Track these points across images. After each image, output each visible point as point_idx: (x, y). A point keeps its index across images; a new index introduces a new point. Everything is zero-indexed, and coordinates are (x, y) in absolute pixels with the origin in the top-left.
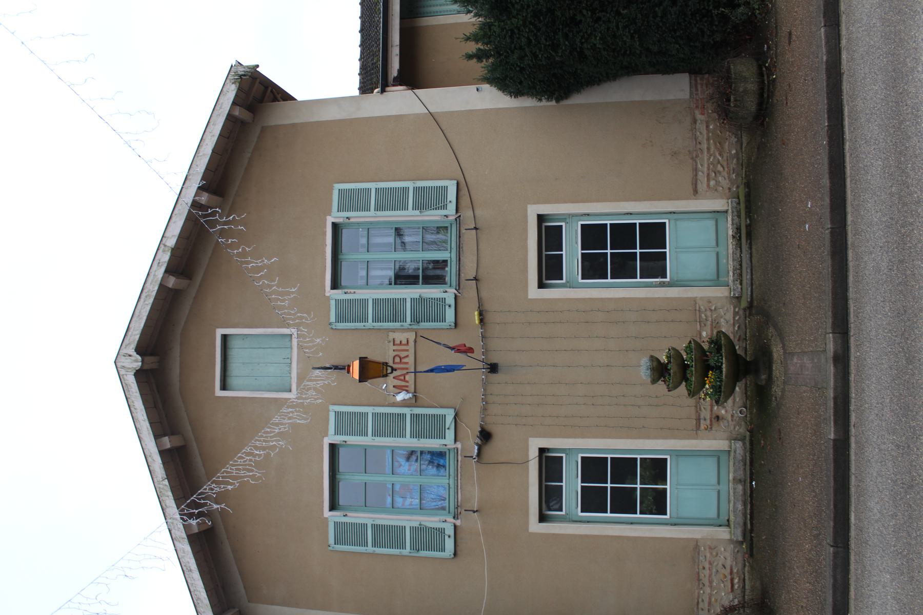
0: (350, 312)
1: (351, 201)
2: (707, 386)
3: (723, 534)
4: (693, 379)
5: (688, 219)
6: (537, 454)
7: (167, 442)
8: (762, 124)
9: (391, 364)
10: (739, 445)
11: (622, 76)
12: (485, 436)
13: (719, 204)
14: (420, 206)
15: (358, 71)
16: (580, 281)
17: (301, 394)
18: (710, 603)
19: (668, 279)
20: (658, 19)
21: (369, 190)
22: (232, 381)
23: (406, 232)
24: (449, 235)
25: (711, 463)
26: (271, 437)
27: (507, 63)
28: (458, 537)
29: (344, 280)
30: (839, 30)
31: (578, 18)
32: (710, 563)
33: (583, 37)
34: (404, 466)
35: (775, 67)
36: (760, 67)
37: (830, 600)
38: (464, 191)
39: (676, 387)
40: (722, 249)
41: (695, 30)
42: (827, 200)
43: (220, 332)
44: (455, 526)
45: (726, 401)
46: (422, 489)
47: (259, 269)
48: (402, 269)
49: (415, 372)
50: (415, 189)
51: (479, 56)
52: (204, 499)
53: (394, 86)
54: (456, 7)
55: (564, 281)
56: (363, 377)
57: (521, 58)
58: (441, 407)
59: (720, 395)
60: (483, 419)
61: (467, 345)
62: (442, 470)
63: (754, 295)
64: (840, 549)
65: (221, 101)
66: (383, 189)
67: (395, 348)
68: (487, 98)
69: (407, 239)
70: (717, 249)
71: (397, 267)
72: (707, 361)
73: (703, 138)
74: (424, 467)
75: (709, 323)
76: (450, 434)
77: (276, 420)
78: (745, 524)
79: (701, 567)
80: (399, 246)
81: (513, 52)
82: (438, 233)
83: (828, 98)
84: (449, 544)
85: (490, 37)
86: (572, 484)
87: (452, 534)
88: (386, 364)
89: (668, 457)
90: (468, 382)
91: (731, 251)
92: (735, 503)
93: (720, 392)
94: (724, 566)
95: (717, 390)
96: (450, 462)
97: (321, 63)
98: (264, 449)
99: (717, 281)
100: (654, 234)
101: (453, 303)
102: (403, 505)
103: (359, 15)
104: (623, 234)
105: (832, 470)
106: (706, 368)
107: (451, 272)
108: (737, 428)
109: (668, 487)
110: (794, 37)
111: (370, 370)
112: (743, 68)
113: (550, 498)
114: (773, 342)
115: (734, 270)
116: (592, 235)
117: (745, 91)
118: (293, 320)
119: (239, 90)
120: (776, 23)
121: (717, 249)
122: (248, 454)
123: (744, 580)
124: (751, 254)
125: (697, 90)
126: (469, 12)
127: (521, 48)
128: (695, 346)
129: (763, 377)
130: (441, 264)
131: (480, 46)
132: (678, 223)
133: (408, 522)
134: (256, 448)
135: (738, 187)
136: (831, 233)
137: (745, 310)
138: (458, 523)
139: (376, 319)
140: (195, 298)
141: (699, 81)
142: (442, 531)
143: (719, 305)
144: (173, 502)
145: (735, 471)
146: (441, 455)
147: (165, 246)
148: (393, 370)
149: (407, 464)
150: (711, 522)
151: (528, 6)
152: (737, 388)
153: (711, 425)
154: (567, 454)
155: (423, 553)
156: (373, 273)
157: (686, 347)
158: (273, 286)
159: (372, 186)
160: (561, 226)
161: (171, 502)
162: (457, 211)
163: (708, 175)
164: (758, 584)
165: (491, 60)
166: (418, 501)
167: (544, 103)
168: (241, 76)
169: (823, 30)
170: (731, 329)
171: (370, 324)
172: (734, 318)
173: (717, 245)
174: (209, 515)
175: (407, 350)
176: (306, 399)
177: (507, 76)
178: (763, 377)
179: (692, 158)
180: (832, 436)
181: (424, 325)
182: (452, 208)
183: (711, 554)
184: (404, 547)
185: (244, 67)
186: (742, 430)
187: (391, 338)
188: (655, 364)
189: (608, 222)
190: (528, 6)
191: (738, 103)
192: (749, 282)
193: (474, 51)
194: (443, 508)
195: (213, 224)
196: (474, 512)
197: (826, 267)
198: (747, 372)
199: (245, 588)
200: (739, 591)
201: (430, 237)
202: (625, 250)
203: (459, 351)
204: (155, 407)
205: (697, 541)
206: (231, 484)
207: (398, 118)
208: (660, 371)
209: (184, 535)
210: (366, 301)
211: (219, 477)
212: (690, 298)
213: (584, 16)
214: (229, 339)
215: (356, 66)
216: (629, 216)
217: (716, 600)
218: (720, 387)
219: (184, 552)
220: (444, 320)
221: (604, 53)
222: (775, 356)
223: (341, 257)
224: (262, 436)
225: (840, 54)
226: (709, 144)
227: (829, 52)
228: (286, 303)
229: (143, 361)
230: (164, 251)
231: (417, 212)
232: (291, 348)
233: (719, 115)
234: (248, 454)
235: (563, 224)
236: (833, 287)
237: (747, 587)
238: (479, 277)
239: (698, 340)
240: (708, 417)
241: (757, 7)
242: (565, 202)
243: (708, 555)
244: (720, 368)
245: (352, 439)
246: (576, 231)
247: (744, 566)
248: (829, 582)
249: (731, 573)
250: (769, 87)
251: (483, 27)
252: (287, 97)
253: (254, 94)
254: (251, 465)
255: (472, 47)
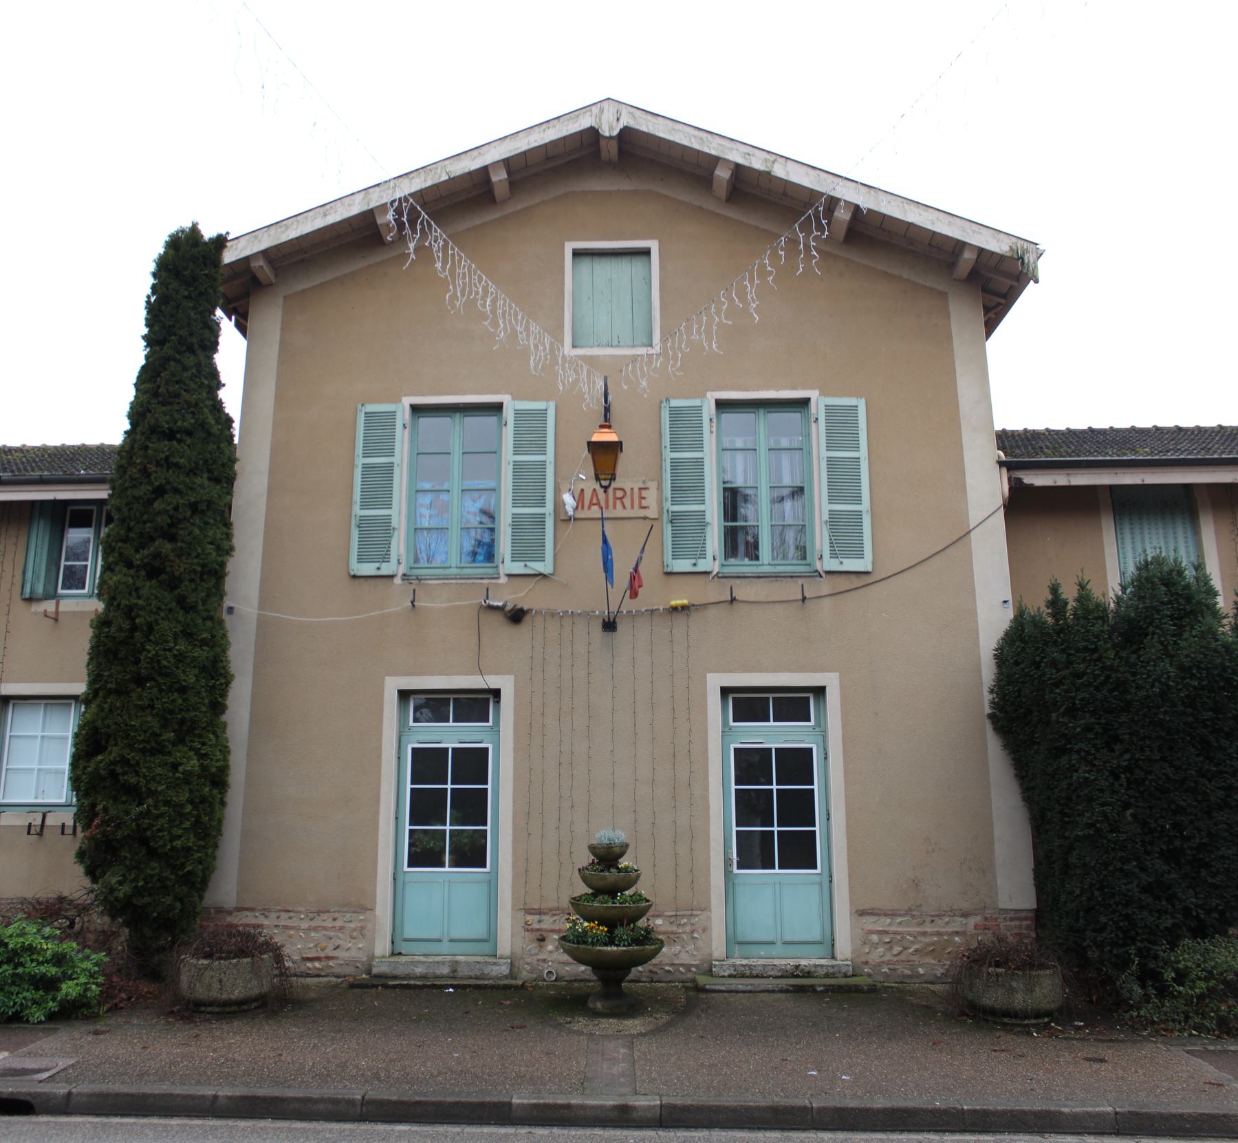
0: (685, 426)
1: (841, 423)
2: (586, 924)
3: (382, 947)
4: (596, 904)
5: (822, 902)
6: (492, 687)
7: (499, 177)
8: (963, 1014)
9: (614, 485)
10: (505, 970)
11: (1030, 809)
12: (517, 616)
13: (845, 949)
14: (834, 520)
15: (1030, 427)
16: (732, 747)
17: (570, 362)
18: (286, 927)
19: (736, 871)
20: (1119, 865)
21: (857, 449)
22: (586, 265)
23: (798, 503)
24: (795, 562)
25: (479, 931)
26: (510, 321)
27: (1046, 644)
28: (378, 580)
29: (729, 417)
30: (1110, 1134)
31: (1118, 747)
32: (341, 928)
33: (1088, 753)
34: (473, 506)
35: (1050, 1037)
36: (1048, 1014)
37: (290, 1093)
38: (857, 582)
39: (584, 879)
40: (779, 949)
41: (1103, 919)
42: (853, 1104)
43: (654, 245)
44: (392, 577)
45: (566, 951)
46: (442, 530)
47: (742, 295)
48: (746, 499)
49: (602, 519)
50: (859, 514)
51: (1056, 603)
52: (422, 229)
53: (1009, 479)
54: (1131, 569)
55: (732, 723)
56: (594, 447)
57: (1054, 664)
58: (555, 556)
59: (574, 943)
60: (539, 612)
61: (640, 591)
62: (469, 559)
63: (714, 995)
64: (359, 1109)
65: (984, 230)
66: (858, 469)
67: (636, 491)
68: (993, 618)
69: (788, 505)
70: (779, 943)
71: (748, 492)
72: (622, 925)
73: (940, 926)
74: (473, 533)
75: (675, 929)
76: (518, 568)
77: (534, 328)
78: (395, 977)
79: (336, 915)
80: (777, 493)
81: (1063, 651)
82: (797, 548)
83: (1004, 1112)
84: (368, 569)
85: (1084, 618)
86: (451, 735)
87: (382, 572)
88: (613, 478)
89: (488, 869)
90: (588, 590)
91: (776, 962)
92: (424, 963)
93: (578, 943)
94: (337, 947)
95: (581, 938)
96: (481, 569)
97: (1045, 372)
98: (494, 312)
99: (733, 941)
100: (800, 852)
101: (699, 569)
102: (421, 505)
103: (1116, 426)
104: (800, 808)
105: (469, 1099)
106: (611, 923)
107: (742, 565)
108: (528, 968)
109: (447, 869)
110: (1096, 1066)
111: (605, 457)
112: (1046, 988)
113: (434, 705)
114: (648, 1019)
115: (750, 967)
116: (797, 764)
117: (1012, 990)
118: (672, 348)
119: (1001, 257)
120: (1117, 1041)
121: (779, 943)
122: (485, 289)
123: (318, 976)
124: (773, 991)
125: (1012, 919)
126: (1124, 588)
127: (1070, 663)
128: (641, 908)
129: (599, 1005)
130: (753, 552)
131: (1072, 604)
132: (817, 887)
133: (398, 512)
134: (494, 301)
135: (869, 975)
136: (805, 1108)
137: (694, 981)
138: (398, 581)
139: (675, 464)
140: (701, 208)
141: (1025, 923)
142: (385, 558)
143: (700, 943)
144: (418, 188)
145: (467, 963)
146: (490, 557)
147: (774, 162)
148: (606, 488)
149: (477, 510)
150: (398, 930)
151: (1134, 674)
152: (583, 968)
153: (532, 930)
154: (491, 727)
155: (355, 533)
156: (739, 457)
157: (640, 895)
158: (720, 317)
159: (863, 453)
160: (809, 720)
161: (417, 184)
162: (828, 573)
163: (887, 932)
164: (313, 995)
165: (1050, 620)
166: (427, 525)
167: (987, 697)
168: (1022, 258)
169: (1110, 1109)
170: (666, 961)
171: (669, 455)
172: (682, 965)
173: (786, 943)
174: (401, 239)
175: (632, 507)
176: (564, 369)
177: (1026, 642)
178: (599, 1005)
179: (910, 910)
180: (515, 1101)
181: (668, 530)
182: (833, 565)
183: (355, 930)
184: (363, 507)
185: (1035, 263)
186: (525, 975)
187: (649, 484)
188: (617, 850)
189: (409, 786)
190: (1134, 674)
191: (993, 979)
192: (733, 987)
193: (1063, 596)
194: (416, 560)
195: (806, 227)
196: (412, 602)
197: (756, 1098)
198: (604, 980)
199: (304, 291)
200: (303, 968)
201: (790, 536)
202: (776, 814)
203: (633, 578)
204: (548, 159)
205: (372, 910)
206: (444, 267)
207: (962, 487)
208: (607, 857)
209: (372, 205)
210: (700, 448)
211: (453, 249)
212: (709, 902)
213: (1121, 755)
214: (645, 258)
215: (1037, 424)
216: (825, 817)
217: (290, 936)
218: (585, 943)
219: (350, 205)
220: (675, 557)
221: (1064, 784)
222: (629, 1023)
223: (762, 411)
224: (511, 308)
225: (1073, 1134)
226: (932, 934)
227: (1075, 1116)
228: (695, 337)
229: (611, 138)
230: (766, 160)
231: (826, 517)
232: (633, 346)
233: (974, 951)
234: (485, 289)
235: (812, 723)
236: (727, 1108)
237: (308, 980)
238: (735, 605)
239: (651, 912)
240: (543, 926)
241: (1142, 1013)
242: (844, 726)
243: (353, 925)
244: (611, 943)
245: (509, 433)
246: (803, 741)
247: (338, 977)
248: (314, 1092)
249: (328, 958)
250: (1020, 1025)
251: (1101, 609)
252: (990, 327)
253: (992, 280)
254: (470, 294)
255: (1069, 593)
